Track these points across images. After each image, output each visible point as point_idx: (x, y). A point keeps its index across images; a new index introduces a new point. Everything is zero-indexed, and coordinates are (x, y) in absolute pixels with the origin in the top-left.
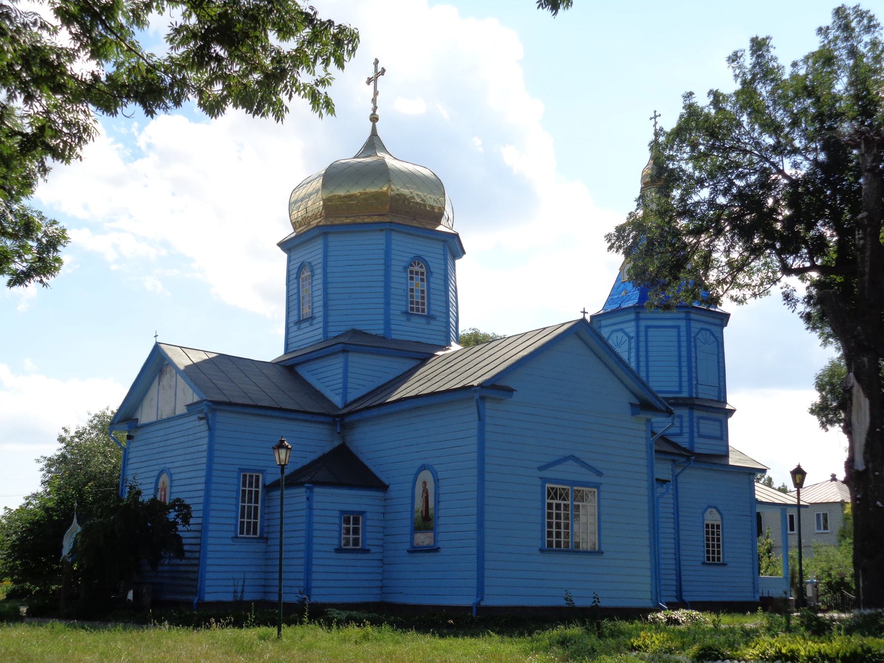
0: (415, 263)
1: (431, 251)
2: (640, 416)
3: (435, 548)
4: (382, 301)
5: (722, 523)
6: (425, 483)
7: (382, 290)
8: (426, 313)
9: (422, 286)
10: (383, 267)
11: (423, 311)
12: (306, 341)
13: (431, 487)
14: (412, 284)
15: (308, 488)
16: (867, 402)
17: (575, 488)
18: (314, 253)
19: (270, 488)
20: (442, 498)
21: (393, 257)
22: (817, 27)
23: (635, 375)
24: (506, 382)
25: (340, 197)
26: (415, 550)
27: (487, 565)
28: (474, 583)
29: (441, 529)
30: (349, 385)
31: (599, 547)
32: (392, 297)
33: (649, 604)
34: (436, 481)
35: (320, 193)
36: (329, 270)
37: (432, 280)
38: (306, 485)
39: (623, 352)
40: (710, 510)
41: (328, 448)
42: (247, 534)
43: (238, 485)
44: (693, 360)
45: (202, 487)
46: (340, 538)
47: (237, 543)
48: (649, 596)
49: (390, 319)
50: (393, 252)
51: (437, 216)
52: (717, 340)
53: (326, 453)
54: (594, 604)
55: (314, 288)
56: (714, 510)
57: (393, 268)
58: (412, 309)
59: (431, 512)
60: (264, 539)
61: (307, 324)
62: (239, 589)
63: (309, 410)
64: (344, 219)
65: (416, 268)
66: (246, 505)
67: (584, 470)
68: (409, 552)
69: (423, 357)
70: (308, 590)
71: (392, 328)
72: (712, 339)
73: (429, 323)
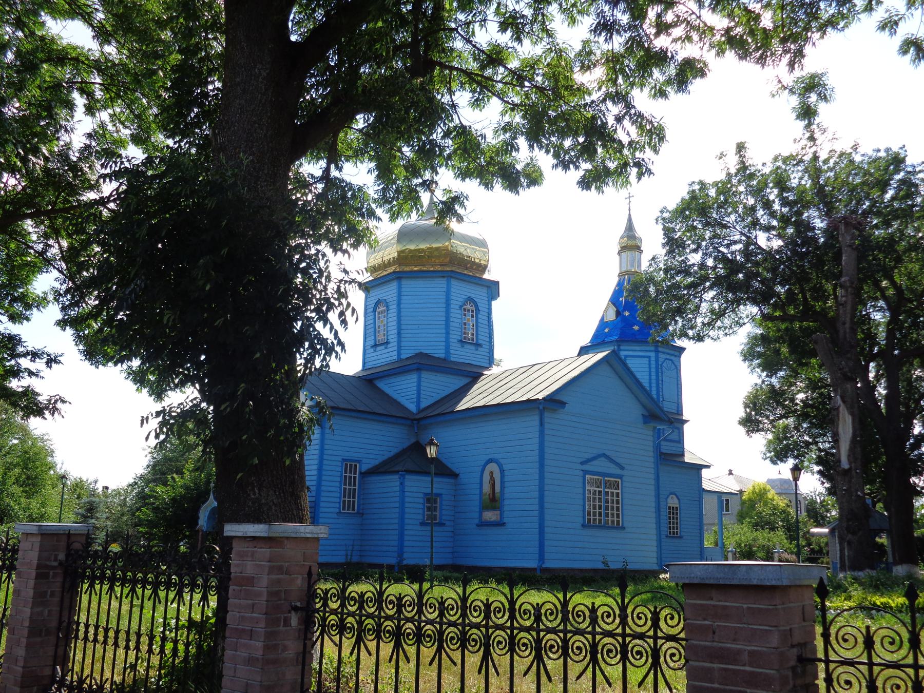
1: (479, 294)
6: (492, 473)
7: (444, 323)
10: (444, 305)
13: (497, 476)
14: (465, 319)
16: (850, 417)
18: (389, 292)
19: (364, 474)
20: (506, 484)
22: (889, 146)
23: (648, 394)
24: (563, 398)
25: (411, 251)
26: (483, 524)
27: (547, 536)
29: (506, 508)
30: (422, 396)
31: (622, 524)
32: (451, 328)
34: (502, 472)
36: (402, 306)
37: (479, 316)
39: (644, 378)
41: (407, 444)
43: (342, 472)
44: (660, 382)
45: (315, 473)
46: (423, 515)
48: (655, 560)
50: (452, 294)
51: (483, 268)
56: (674, 496)
57: (452, 306)
59: (497, 495)
60: (360, 514)
61: (383, 347)
62: (349, 553)
63: (394, 414)
66: (347, 487)
67: (613, 466)
68: (478, 525)
69: (474, 376)
70: (401, 554)
72: (673, 367)
73: (477, 350)
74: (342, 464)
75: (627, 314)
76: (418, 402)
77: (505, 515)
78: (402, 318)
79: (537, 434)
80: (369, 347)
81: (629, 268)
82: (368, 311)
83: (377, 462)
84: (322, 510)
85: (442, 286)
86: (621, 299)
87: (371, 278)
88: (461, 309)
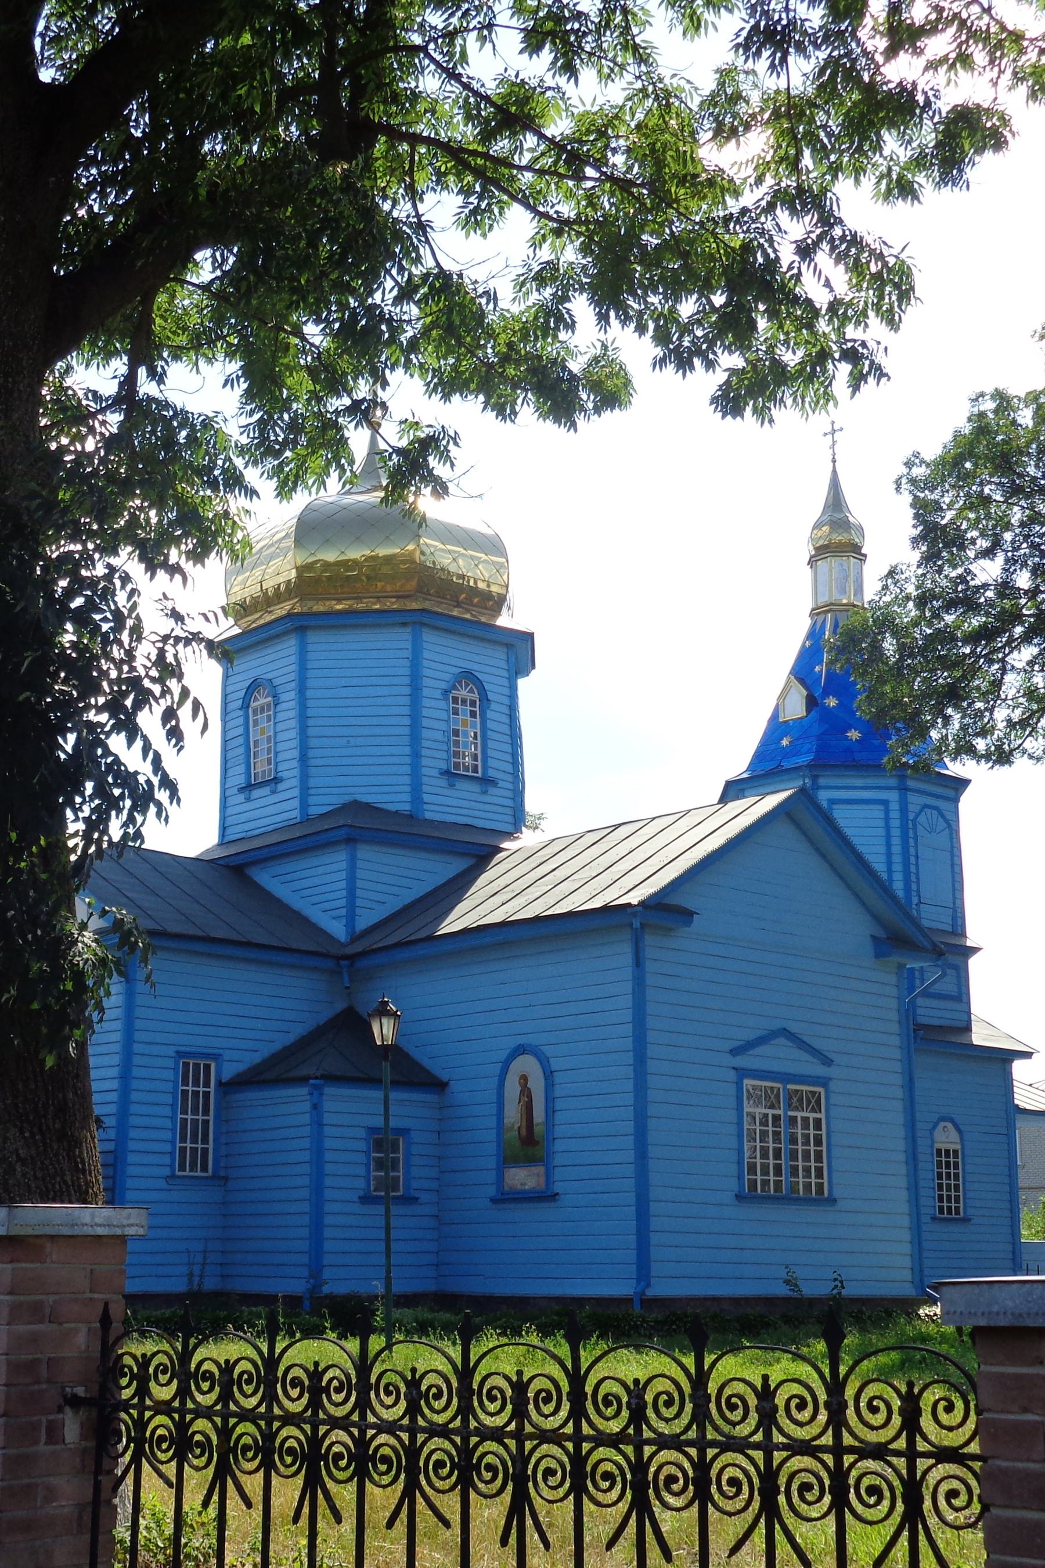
0: (460, 683)
2: (890, 959)
3: (549, 1193)
4: (407, 750)
5: (963, 1148)
6: (524, 1079)
7: (407, 731)
8: (480, 775)
9: (474, 726)
10: (407, 690)
11: (475, 769)
12: (267, 821)
13: (537, 1085)
14: (456, 722)
15: (314, 1086)
17: (789, 1087)
19: (227, 1087)
20: (559, 1105)
21: (426, 672)
23: (884, 889)
25: (327, 565)
26: (507, 1198)
28: (632, 1255)
29: (558, 1160)
30: (359, 902)
31: (830, 1191)
32: (425, 743)
33: (908, 1291)
34: (549, 1075)
35: (290, 554)
36: (309, 693)
37: (489, 714)
38: (312, 1081)
40: (942, 1124)
41: (325, 1014)
42: (191, 1170)
44: (913, 860)
45: (115, 1084)
47: (175, 1187)
48: (907, 1275)
49: (422, 784)
50: (425, 663)
51: (497, 602)
52: (949, 826)
53: (321, 1023)
54: (835, 1292)
55: (280, 727)
56: (949, 1125)
57: (426, 692)
58: (457, 766)
59: (538, 1130)
60: (221, 1179)
61: (266, 790)
62: (197, 1270)
63: (294, 946)
64: (334, 602)
65: (463, 693)
66: (189, 1117)
67: (805, 1056)
68: (493, 1200)
71: (425, 800)
73: (485, 792)
74: (177, 1064)
75: (832, 702)
76: (351, 917)
77: (558, 1174)
78: (310, 722)
79: (628, 987)
80: (235, 791)
81: (836, 597)
82: (231, 707)
83: (257, 1058)
84: (131, 1170)
85: (402, 645)
86: (817, 669)
87: (236, 631)
88: (446, 699)
